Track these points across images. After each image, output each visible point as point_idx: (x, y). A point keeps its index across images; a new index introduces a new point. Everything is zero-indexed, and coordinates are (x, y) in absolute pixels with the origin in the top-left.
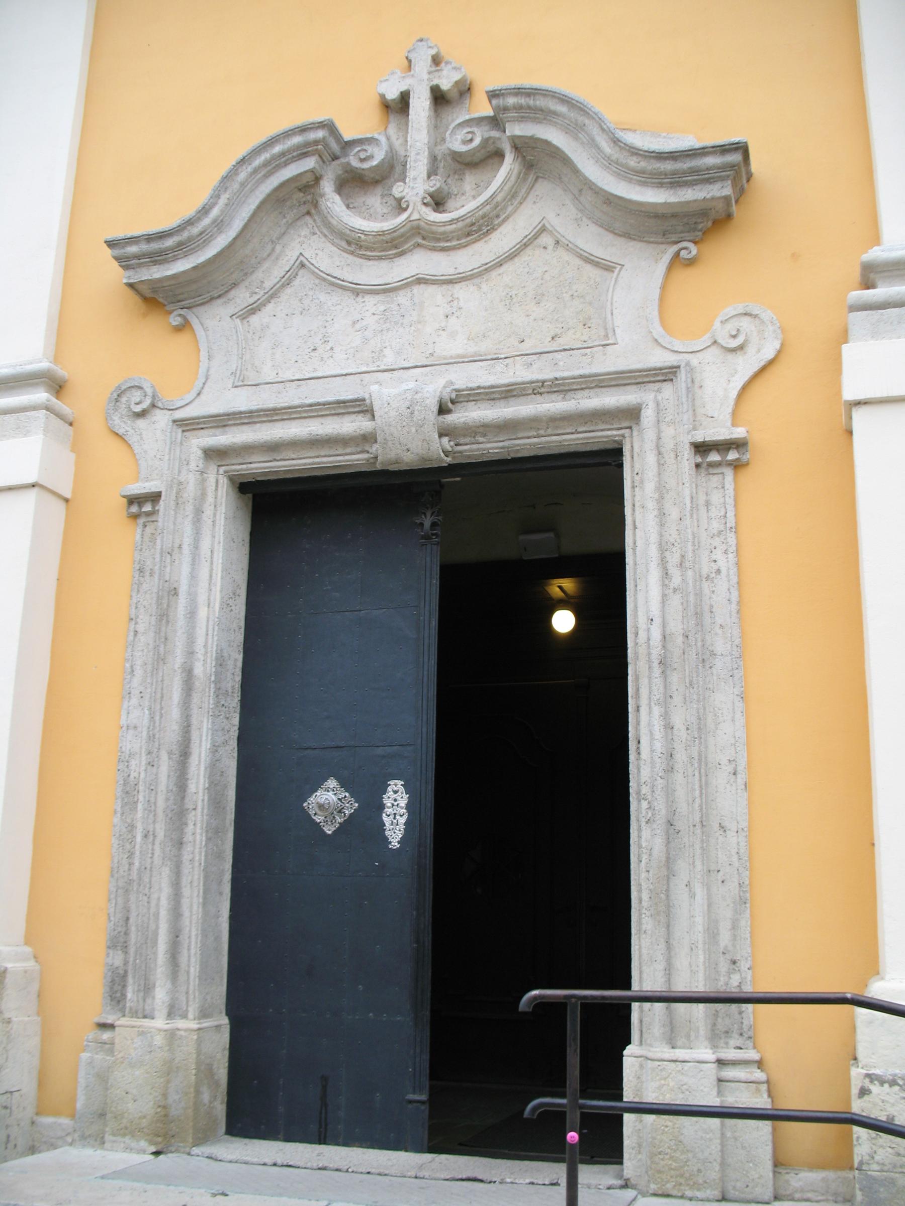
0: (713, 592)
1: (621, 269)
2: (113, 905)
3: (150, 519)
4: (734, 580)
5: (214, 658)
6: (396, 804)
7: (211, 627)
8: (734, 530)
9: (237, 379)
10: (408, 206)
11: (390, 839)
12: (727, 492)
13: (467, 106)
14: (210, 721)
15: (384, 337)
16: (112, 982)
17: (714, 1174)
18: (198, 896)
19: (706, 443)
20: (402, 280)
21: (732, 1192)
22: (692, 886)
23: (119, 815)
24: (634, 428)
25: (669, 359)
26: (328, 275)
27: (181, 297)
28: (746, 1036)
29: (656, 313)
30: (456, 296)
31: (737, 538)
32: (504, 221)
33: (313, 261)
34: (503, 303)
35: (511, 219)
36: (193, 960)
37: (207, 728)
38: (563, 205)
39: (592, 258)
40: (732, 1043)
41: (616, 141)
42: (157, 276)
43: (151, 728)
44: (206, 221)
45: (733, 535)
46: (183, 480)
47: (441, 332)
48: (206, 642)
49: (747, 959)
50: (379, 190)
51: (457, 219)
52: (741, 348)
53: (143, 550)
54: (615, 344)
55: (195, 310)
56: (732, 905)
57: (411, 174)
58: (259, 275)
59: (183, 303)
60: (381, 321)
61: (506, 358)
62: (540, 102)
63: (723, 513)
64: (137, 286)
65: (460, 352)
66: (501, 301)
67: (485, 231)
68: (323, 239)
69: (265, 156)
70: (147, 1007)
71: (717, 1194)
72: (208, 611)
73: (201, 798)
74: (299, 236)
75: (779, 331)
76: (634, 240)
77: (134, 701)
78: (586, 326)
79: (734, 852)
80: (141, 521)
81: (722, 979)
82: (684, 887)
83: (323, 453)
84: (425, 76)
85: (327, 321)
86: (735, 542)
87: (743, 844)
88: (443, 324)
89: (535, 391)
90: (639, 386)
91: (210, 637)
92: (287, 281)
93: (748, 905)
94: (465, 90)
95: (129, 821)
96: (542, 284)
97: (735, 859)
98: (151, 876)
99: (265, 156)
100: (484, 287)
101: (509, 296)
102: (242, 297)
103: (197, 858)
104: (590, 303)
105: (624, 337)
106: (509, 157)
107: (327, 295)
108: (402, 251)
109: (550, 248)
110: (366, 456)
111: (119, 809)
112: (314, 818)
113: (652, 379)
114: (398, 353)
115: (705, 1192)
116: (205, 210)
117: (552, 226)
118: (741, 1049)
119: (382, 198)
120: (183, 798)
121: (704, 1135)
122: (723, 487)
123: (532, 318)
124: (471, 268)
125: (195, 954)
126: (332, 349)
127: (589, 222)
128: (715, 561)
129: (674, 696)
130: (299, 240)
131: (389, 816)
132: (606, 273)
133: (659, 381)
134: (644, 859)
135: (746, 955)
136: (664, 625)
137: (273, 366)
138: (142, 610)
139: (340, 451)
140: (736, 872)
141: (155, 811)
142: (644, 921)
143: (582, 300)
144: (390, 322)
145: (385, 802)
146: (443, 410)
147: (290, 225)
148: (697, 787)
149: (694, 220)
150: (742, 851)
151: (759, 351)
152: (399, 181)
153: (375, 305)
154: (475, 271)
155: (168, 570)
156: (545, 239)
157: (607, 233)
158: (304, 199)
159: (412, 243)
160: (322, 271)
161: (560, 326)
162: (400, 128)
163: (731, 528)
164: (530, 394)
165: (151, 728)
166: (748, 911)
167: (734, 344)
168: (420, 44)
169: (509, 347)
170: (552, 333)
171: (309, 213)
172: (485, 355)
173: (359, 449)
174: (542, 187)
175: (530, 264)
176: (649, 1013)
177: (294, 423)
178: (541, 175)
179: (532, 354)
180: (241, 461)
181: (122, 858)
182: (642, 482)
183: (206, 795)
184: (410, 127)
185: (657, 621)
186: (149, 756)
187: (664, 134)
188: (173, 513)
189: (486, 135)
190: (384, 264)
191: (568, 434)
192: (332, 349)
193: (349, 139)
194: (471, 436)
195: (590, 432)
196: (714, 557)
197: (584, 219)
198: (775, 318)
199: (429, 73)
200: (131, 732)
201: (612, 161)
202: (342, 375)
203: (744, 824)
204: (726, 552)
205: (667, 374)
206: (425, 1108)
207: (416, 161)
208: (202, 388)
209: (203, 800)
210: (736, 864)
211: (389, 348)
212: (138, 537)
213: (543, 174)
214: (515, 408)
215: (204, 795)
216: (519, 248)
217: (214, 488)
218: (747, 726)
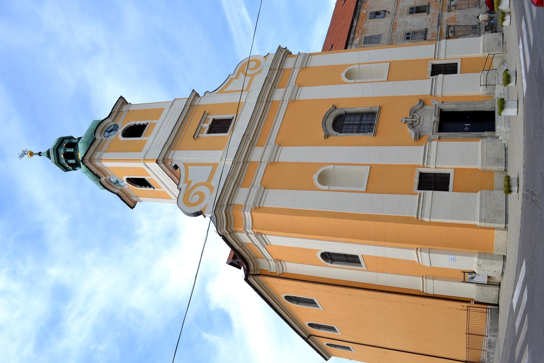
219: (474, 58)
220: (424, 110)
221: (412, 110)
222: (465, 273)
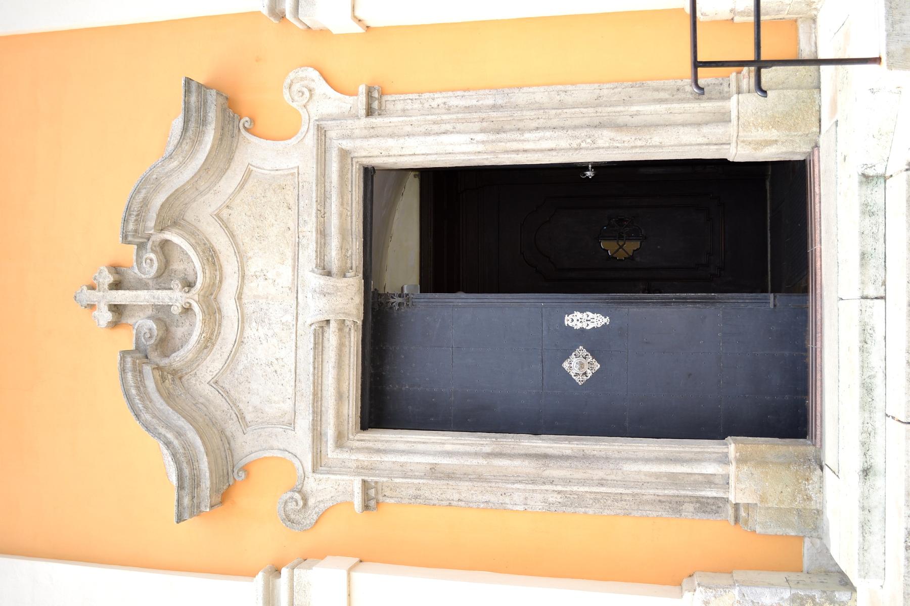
0: (457, 106)
1: (251, 165)
2: (651, 512)
3: (380, 492)
4: (450, 94)
5: (480, 439)
6: (580, 320)
7: (458, 442)
8: (420, 94)
9: (289, 428)
10: (188, 303)
11: (603, 323)
12: (397, 99)
13: (125, 269)
14: (523, 441)
15: (274, 322)
16: (705, 513)
17: (804, 93)
18: (643, 446)
19: (367, 108)
20: (238, 310)
21: (814, 84)
22: (633, 113)
23: (587, 510)
24: (352, 156)
25: (312, 131)
26: (225, 363)
27: (225, 471)
28: (722, 81)
29: (282, 142)
30: (253, 274)
31: (425, 92)
32: (208, 241)
33: (215, 374)
34: (262, 241)
35: (208, 237)
36: (687, 449)
37: (528, 442)
38: (204, 202)
39: (241, 183)
40: (726, 89)
41: (171, 157)
42: (208, 483)
43: (527, 482)
44: (176, 443)
45: (423, 95)
46: (355, 465)
47: (276, 283)
48: (468, 444)
49: (676, 82)
50: (173, 329)
51: (203, 268)
52: (310, 91)
53: (402, 496)
54: (298, 168)
55: (235, 463)
56: (644, 91)
57: (167, 301)
58: (218, 414)
59: (230, 470)
60: (263, 324)
61: (299, 237)
62: (136, 207)
63: (410, 101)
64: (213, 503)
65: (290, 269)
66: (261, 243)
67: (213, 253)
68: (200, 367)
69: (137, 400)
70: (721, 483)
71: (816, 91)
72: (448, 444)
73: (575, 445)
74: (195, 385)
75: (302, 68)
76: (233, 156)
77: (507, 500)
78: (284, 187)
79: (612, 91)
80: (381, 498)
81: (688, 96)
82: (633, 119)
83: (347, 362)
84: (101, 294)
85: (257, 364)
86: (428, 94)
87: (608, 86)
88: (271, 281)
89: (323, 216)
90: (327, 151)
91: (465, 442)
92: (225, 393)
93: (644, 82)
94: (115, 269)
95: (591, 502)
96: (254, 217)
97: (616, 90)
98: (629, 481)
99: (137, 400)
100: (249, 255)
101: (258, 238)
102: (232, 427)
103: (617, 447)
104: (270, 185)
105: (294, 171)
106: (167, 235)
107: (239, 364)
108: (218, 309)
109: (230, 211)
110: (352, 331)
111: (583, 510)
112: (589, 377)
113: (323, 143)
114: (286, 311)
115: (815, 98)
116: (168, 444)
117: (217, 210)
118: (729, 84)
119: (179, 327)
120: (576, 457)
121: (782, 99)
122: (394, 101)
123: (275, 222)
124: (236, 262)
125: (683, 448)
126: (277, 359)
127: (218, 185)
128: (438, 105)
129: (518, 127)
130: (198, 385)
131: (588, 325)
132: (252, 176)
133: (325, 139)
134: (616, 145)
135: (673, 82)
136: (474, 132)
137: (283, 402)
138: (444, 496)
139: (347, 350)
140: (624, 90)
141: (584, 479)
142: (654, 144)
143: (267, 191)
144: (265, 318)
145: (579, 328)
146: (329, 274)
147: (187, 390)
148: (573, 110)
149: (227, 117)
150: (612, 86)
151: (313, 80)
152: (169, 311)
153: (251, 329)
154: (239, 259)
155: (416, 474)
156: (225, 213)
157: (227, 174)
158: (170, 381)
159: (213, 302)
160: (223, 367)
161: (282, 204)
162: (133, 315)
163: (419, 96)
164: (324, 220)
165: (527, 482)
166: (649, 82)
167: (307, 94)
168: (77, 299)
169: (292, 237)
170: (287, 209)
171: (180, 378)
172: (295, 253)
173: (347, 336)
174: (190, 216)
175: (239, 224)
176: (710, 138)
177: (325, 382)
178: (182, 217)
179: (298, 221)
180: (346, 422)
181: (618, 506)
182: (387, 149)
183: (573, 443)
184: (135, 303)
185: (473, 136)
186: (546, 483)
187: (169, 139)
188: (377, 472)
189: (149, 250)
190: (224, 322)
191: (352, 197)
192: (277, 359)
193: (134, 346)
194: (347, 259)
195: (352, 183)
196: (436, 106)
197: (215, 189)
198: (295, 71)
199: (99, 291)
200: (529, 502)
201: (183, 161)
202: (296, 350)
203: (596, 86)
204: (433, 99)
205: (321, 132)
206: (778, 295)
207: (158, 299)
208: (292, 454)
209: (577, 444)
210: (620, 89)
211: (281, 319)
212: (392, 501)
213: (181, 215)
214: (333, 227)
215: (574, 444)
216: (228, 231)
217: (363, 442)
218: (538, 86)
219: (570, 15)
220: (242, 185)
221: (145, 203)
222: (699, 59)
